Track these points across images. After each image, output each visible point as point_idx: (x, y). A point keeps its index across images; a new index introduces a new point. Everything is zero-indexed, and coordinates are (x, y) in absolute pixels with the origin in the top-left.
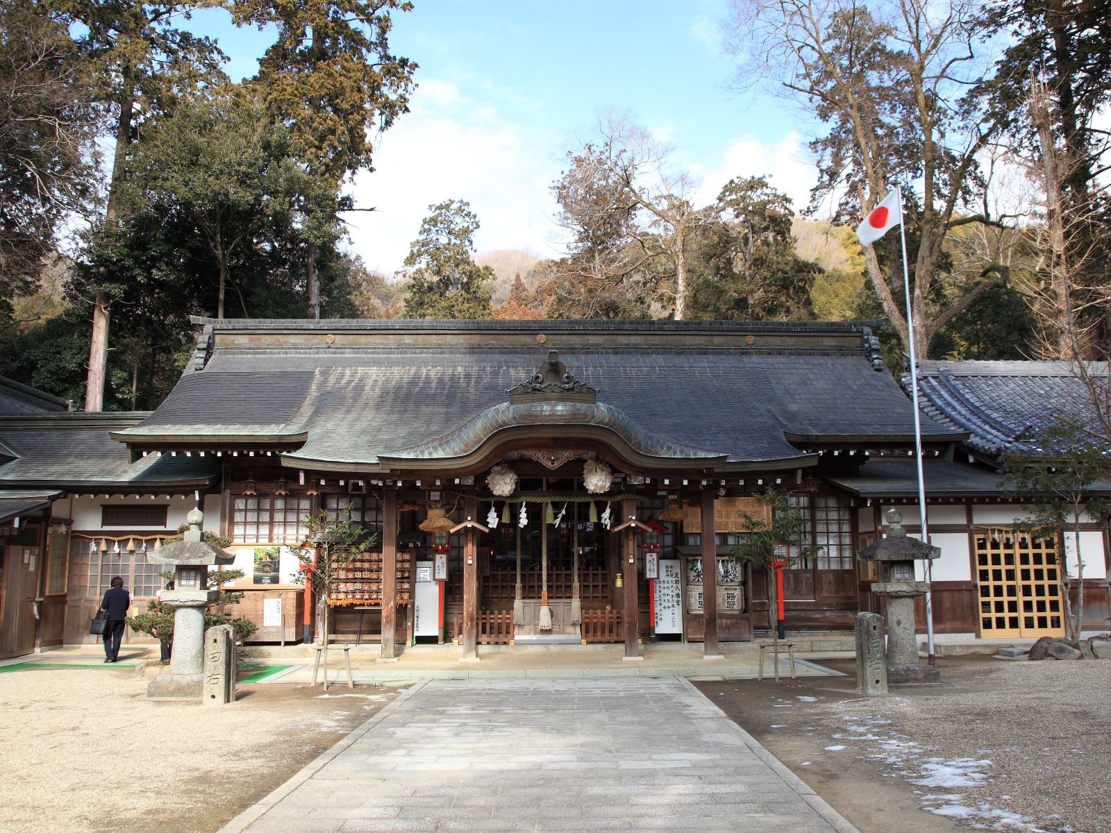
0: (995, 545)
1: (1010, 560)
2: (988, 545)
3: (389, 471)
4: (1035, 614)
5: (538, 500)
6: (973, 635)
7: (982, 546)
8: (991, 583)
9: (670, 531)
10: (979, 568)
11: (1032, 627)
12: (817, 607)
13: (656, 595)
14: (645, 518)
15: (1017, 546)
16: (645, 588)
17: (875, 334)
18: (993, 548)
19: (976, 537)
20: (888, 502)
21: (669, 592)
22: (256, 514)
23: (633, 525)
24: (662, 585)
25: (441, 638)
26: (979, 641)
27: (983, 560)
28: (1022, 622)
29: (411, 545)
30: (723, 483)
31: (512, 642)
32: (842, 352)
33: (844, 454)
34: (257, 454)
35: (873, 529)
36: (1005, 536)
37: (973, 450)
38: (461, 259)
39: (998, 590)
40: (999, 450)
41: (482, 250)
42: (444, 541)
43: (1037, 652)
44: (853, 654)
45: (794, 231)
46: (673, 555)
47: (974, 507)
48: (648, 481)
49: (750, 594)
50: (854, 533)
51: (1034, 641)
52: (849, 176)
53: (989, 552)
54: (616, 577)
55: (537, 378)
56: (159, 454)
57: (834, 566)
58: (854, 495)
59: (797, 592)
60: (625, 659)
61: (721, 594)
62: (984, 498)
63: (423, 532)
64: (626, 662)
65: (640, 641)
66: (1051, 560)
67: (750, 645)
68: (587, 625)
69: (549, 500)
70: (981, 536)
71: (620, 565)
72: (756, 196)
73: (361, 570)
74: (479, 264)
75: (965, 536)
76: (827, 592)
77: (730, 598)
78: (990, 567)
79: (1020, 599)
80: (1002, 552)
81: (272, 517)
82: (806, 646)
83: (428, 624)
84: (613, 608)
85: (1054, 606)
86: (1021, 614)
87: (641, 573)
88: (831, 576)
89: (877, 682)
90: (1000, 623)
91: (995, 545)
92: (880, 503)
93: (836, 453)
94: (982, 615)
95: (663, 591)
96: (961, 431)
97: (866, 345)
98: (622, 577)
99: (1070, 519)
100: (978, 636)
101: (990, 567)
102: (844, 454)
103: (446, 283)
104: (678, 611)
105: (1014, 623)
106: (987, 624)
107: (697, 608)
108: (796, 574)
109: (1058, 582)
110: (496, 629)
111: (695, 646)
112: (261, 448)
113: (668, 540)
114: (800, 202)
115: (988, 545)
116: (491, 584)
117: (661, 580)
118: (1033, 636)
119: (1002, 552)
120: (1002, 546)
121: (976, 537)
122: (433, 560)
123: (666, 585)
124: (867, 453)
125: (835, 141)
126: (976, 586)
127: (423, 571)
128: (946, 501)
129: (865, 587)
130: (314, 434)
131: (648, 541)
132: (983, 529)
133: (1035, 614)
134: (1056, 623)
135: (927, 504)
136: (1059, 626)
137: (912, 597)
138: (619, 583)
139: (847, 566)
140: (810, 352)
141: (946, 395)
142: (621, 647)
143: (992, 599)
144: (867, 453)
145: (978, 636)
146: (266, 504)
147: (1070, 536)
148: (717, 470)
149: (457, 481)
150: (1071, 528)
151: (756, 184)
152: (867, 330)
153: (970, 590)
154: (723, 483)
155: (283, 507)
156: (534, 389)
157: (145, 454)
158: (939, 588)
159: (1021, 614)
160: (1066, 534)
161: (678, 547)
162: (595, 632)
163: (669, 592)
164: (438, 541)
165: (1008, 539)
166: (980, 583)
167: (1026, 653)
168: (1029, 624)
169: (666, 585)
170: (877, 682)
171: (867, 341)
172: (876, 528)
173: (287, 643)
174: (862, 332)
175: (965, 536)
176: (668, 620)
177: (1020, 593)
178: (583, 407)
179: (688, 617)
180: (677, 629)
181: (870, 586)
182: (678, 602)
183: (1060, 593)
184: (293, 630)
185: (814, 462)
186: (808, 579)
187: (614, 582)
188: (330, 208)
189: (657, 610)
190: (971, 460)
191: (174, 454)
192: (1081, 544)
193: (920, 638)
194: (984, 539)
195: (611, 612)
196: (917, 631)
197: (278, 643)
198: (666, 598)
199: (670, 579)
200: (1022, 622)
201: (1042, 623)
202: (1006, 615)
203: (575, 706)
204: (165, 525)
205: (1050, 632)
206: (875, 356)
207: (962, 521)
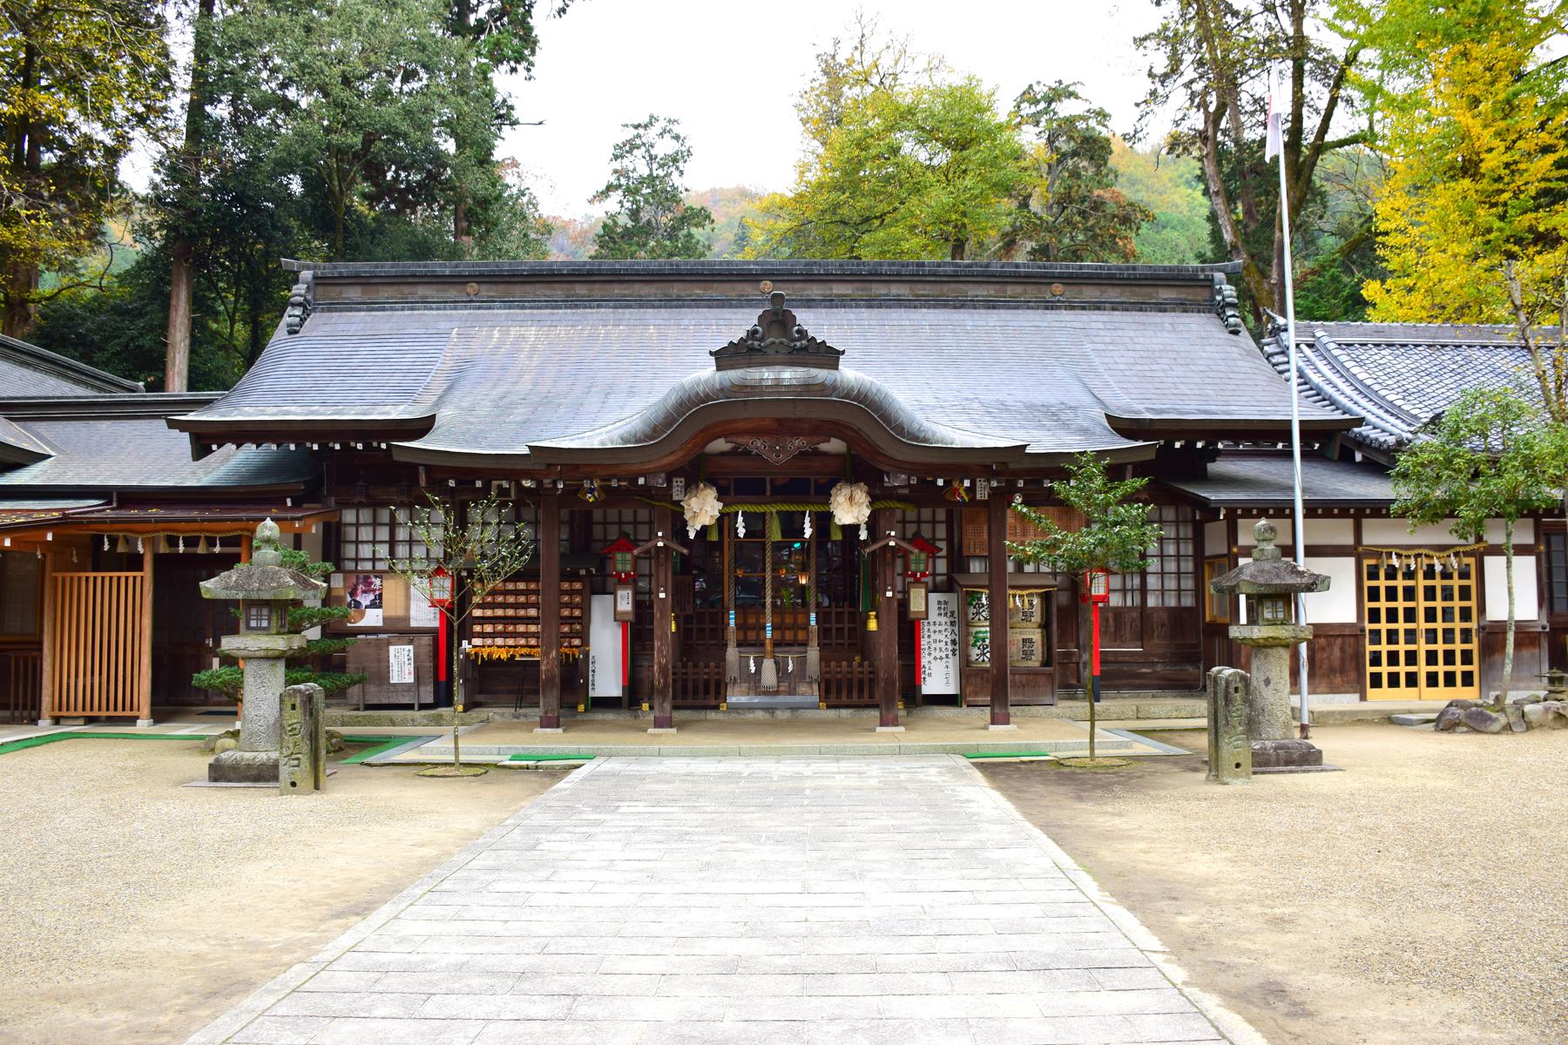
0: (1392, 574)
1: (1410, 593)
2: (1382, 574)
3: (527, 451)
4: (1441, 668)
5: (793, 508)
6: (1357, 696)
7: (1373, 575)
8: (1384, 626)
9: (944, 553)
10: (1368, 605)
11: (1436, 685)
12: (1144, 660)
13: (924, 642)
14: (909, 535)
15: (1420, 575)
16: (909, 633)
17: (1229, 282)
18: (1388, 577)
19: (1366, 562)
20: (1247, 514)
21: (942, 637)
22: (370, 529)
23: (892, 543)
24: (932, 628)
25: (625, 702)
26: (1364, 706)
27: (1374, 594)
28: (1422, 679)
29: (583, 572)
30: (1021, 484)
31: (724, 707)
32: (1184, 307)
33: (1189, 446)
34: (367, 446)
35: (1225, 551)
36: (1405, 561)
37: (1363, 443)
38: (667, 198)
39: (1392, 637)
40: (1400, 443)
41: (695, 182)
42: (629, 567)
43: (1444, 723)
44: (1204, 722)
45: (1112, 161)
46: (948, 587)
47: (1366, 522)
48: (914, 481)
49: (1055, 640)
50: (1199, 557)
51: (1443, 704)
52: (1188, 85)
53: (1382, 583)
54: (868, 617)
55: (755, 332)
56: (274, 447)
57: (1171, 602)
58: (1203, 504)
59: (1117, 637)
60: (879, 729)
61: (1015, 638)
62: (1250, 510)
63: (214, 603)
64: (881, 734)
65: (900, 705)
66: (1465, 593)
67: (1053, 709)
68: (828, 683)
69: (774, 509)
70: (1373, 562)
71: (873, 601)
72: (1065, 108)
73: (504, 606)
74: (690, 200)
75: (1351, 561)
76: (1158, 644)
77: (1027, 635)
78: (1383, 605)
79: (1422, 647)
80: (1400, 583)
81: (392, 534)
82: (1130, 712)
83: (607, 680)
84: (863, 659)
85: (1467, 657)
86: (1422, 669)
87: (904, 604)
88: (1165, 616)
89: (1238, 765)
90: (1394, 681)
91: (1392, 574)
92: (1236, 514)
93: (1178, 445)
94: (1370, 669)
95: (934, 637)
96: (1337, 416)
97: (1219, 298)
98: (877, 617)
99: (1494, 537)
100: (1363, 698)
101: (1383, 605)
102: (1189, 446)
103: (648, 230)
104: (953, 664)
105: (1412, 680)
106: (1376, 681)
107: (980, 656)
108: (1118, 613)
109: (1473, 625)
110: (701, 687)
111: (976, 711)
112: (375, 439)
113: (942, 566)
114: (1119, 125)
115: (1382, 574)
116: (695, 626)
117: (931, 619)
118: (1439, 698)
119: (1400, 583)
120: (1400, 576)
121: (1366, 562)
122: (614, 593)
123: (937, 628)
124: (1220, 446)
125: (1170, 39)
126: (1363, 630)
127: (601, 608)
128: (1328, 514)
129: (1219, 630)
130: (444, 415)
131: (913, 567)
132: (1376, 552)
133: (1441, 668)
134: (1468, 679)
135: (1305, 516)
136: (1471, 684)
137: (1286, 646)
138: (873, 625)
139: (1188, 601)
140: (1140, 307)
141: (1325, 370)
142: (875, 713)
143: (1384, 648)
144: (1220, 446)
145: (1363, 698)
146: (384, 515)
147: (1494, 564)
148: (1012, 466)
149: (641, 481)
150: (1496, 550)
151: (1060, 93)
152: (1219, 276)
153: (1356, 636)
154: (1021, 484)
155: (370, 520)
156: (751, 350)
157: (214, 447)
158: (1322, 632)
159: (1422, 669)
160: (1488, 560)
161: (956, 576)
162: (839, 692)
163: (942, 637)
164: (619, 567)
165: (1408, 566)
166: (1369, 626)
167: (1428, 721)
168: (1432, 680)
169: (937, 628)
170: (1238, 765)
171: (1220, 291)
172: (1229, 549)
173: (423, 707)
174: (1212, 280)
175: (1351, 561)
176: (938, 677)
177: (1422, 641)
178: (821, 375)
179: (967, 671)
180: (951, 689)
181: (1227, 632)
182: (954, 651)
183: (1475, 640)
184: (430, 688)
185: (1151, 456)
186: (1133, 620)
187: (865, 624)
188: (483, 120)
189: (924, 661)
190: (1358, 457)
191: (292, 447)
192: (1514, 573)
193: (1295, 700)
194: (1376, 567)
195: (861, 665)
196: (1292, 693)
197: (410, 707)
198: (938, 645)
199: (943, 619)
200: (1422, 679)
201: (1450, 680)
202: (1402, 669)
203: (806, 802)
204: (1309, 693)
205: (1470, 694)
206: (1230, 313)
207: (1349, 540)
